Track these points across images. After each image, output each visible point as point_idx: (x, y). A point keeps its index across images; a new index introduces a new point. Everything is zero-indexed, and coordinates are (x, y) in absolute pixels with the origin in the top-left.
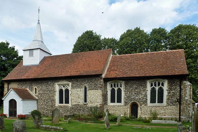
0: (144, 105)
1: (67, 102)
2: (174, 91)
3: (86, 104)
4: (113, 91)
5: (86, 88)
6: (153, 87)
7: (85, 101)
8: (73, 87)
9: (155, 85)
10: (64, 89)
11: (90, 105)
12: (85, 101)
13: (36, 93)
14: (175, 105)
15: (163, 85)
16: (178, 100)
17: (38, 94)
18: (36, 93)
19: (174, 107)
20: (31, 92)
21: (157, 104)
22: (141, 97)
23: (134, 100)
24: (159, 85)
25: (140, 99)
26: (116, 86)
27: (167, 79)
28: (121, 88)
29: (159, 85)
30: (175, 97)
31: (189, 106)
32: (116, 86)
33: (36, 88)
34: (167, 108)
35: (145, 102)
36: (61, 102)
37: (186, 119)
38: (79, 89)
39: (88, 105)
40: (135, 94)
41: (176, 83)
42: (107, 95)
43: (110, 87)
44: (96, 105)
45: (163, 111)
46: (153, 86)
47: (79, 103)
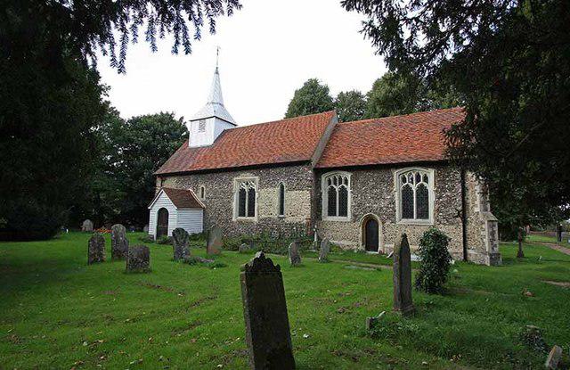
1: (252, 214)
2: (449, 194)
3: (281, 218)
4: (332, 193)
5: (282, 187)
7: (282, 213)
8: (261, 186)
11: (289, 219)
12: (282, 213)
14: (453, 224)
15: (426, 179)
19: (451, 227)
21: (415, 220)
24: (418, 180)
25: (381, 208)
29: (418, 180)
36: (242, 213)
44: (298, 220)
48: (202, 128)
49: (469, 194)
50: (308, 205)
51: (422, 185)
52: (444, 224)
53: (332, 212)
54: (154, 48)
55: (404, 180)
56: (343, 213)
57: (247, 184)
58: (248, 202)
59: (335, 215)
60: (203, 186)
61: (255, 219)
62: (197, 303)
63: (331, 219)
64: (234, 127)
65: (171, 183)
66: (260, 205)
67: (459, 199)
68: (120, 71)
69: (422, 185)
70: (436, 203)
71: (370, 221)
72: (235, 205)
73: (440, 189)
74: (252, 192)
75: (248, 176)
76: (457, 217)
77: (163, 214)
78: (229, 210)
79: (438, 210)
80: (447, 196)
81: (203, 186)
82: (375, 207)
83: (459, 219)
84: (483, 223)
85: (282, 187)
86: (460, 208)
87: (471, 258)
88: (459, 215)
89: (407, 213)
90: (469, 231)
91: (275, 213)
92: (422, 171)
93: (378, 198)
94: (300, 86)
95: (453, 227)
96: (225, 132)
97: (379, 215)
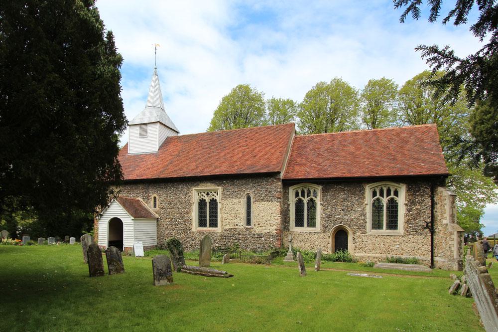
0: (361, 232)
1: (214, 224)
2: (419, 207)
3: (249, 229)
4: (299, 205)
5: (249, 199)
6: (378, 199)
7: (249, 222)
9: (303, 195)
10: (207, 199)
11: (257, 230)
12: (249, 222)
13: (155, 206)
14: (421, 234)
15: (396, 193)
16: (428, 224)
17: (160, 208)
18: (155, 206)
19: (419, 237)
20: (146, 205)
22: (353, 216)
23: (341, 223)
24: (389, 194)
25: (352, 220)
26: (306, 194)
27: (403, 183)
28: (314, 199)
29: (389, 194)
30: (422, 218)
31: (450, 238)
32: (306, 194)
33: (155, 198)
34: (406, 239)
35: (362, 227)
36: (202, 223)
37: (446, 263)
38: (237, 200)
39: (253, 231)
40: (343, 210)
41: (424, 191)
42: (289, 211)
43: (294, 196)
45: (398, 246)
46: (376, 195)
47: (236, 227)
48: (144, 134)
49: (438, 208)
50: (278, 216)
51: (392, 199)
52: (413, 235)
53: (299, 222)
54: (402, 21)
55: (374, 194)
56: (311, 223)
57: (208, 194)
58: (209, 213)
59: (205, 226)
60: (155, 195)
61: (218, 230)
62: (478, 297)
63: (299, 229)
64: (173, 134)
65: (125, 193)
66: (224, 215)
67: (428, 212)
68: (416, 49)
69: (392, 199)
70: (406, 215)
71: (341, 230)
72: (402, 211)
73: (411, 203)
74: (214, 203)
75: (209, 186)
76: (426, 228)
77: (116, 226)
78: (188, 221)
79: (408, 222)
80: (417, 209)
81: (155, 195)
82: (345, 219)
83: (427, 230)
84: (451, 234)
85: (249, 199)
86: (429, 220)
87: (437, 265)
88: (427, 227)
89: (377, 225)
90: (436, 242)
91: (241, 223)
92: (393, 186)
93: (350, 209)
94: (227, 92)
95: (422, 237)
96: (168, 138)
97: (349, 226)
